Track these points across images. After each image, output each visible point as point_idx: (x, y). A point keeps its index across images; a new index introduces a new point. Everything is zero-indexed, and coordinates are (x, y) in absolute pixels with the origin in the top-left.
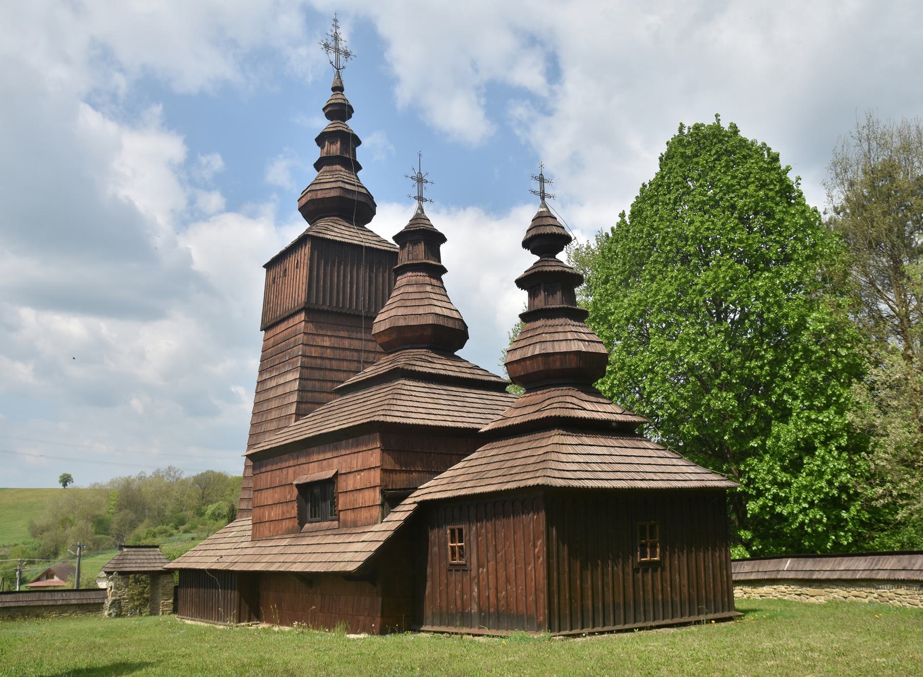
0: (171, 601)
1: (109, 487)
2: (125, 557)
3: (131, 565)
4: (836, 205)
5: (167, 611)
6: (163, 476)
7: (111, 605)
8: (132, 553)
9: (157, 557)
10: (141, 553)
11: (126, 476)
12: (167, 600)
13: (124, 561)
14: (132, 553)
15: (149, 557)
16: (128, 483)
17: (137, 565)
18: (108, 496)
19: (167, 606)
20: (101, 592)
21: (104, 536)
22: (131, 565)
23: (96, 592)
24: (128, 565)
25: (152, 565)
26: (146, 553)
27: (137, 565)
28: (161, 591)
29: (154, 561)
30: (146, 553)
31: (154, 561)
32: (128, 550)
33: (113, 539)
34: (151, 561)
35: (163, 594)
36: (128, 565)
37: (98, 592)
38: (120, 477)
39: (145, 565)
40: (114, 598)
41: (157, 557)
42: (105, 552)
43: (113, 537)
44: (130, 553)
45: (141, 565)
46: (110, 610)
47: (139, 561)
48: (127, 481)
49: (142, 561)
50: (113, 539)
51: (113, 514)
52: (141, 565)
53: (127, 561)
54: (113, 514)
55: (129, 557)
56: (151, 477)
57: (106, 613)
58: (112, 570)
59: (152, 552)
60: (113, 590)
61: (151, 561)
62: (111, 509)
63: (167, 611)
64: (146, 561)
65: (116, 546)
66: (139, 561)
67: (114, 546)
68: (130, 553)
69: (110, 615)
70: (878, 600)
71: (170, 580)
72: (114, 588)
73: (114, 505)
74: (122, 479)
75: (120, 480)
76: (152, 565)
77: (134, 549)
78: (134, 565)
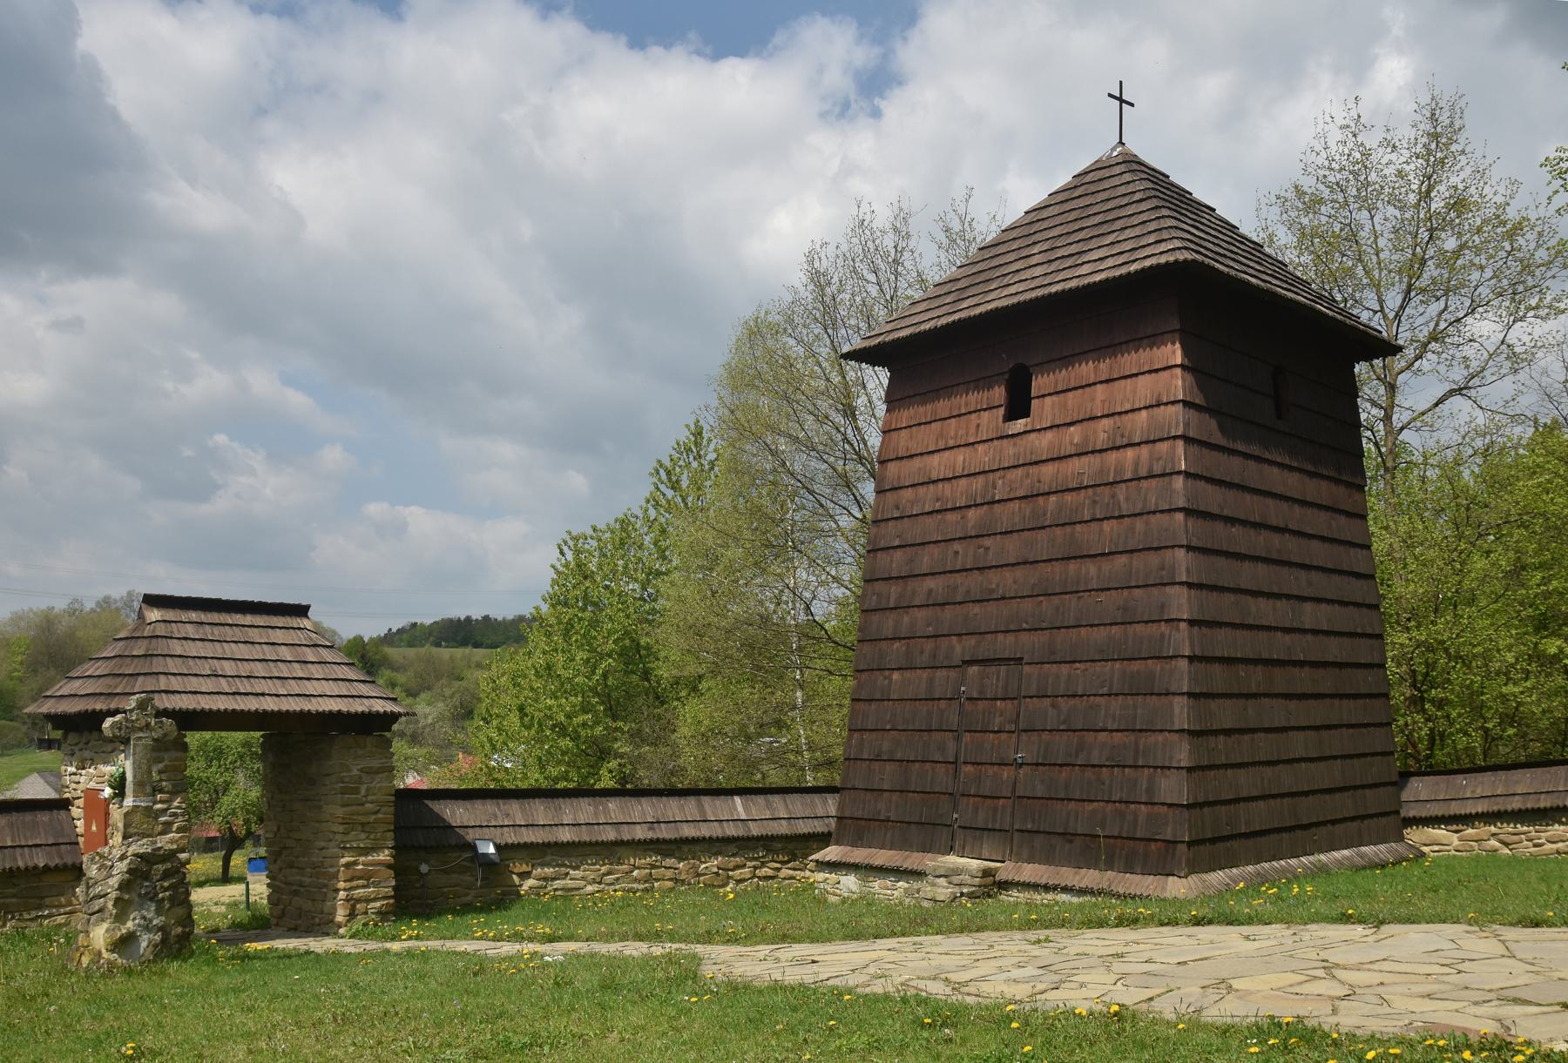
0: (385, 856)
1: (9, 629)
2: (161, 647)
3: (194, 684)
4: (1365, 109)
5: (368, 901)
6: (117, 609)
7: (123, 886)
8: (190, 631)
9: (310, 655)
10: (229, 633)
11: (44, 607)
12: (365, 851)
13: (158, 664)
14: (190, 631)
15: (269, 652)
16: (48, 621)
17: (224, 685)
18: (8, 645)
19: (366, 876)
20: (43, 817)
21: (8, 723)
22: (194, 684)
23: (15, 817)
24: (175, 684)
25: (295, 687)
26: (254, 635)
27: (224, 685)
28: (336, 809)
29: (298, 671)
30: (254, 635)
31: (298, 671)
32: (170, 615)
33: (24, 729)
34: (284, 670)
35: (349, 824)
36: (175, 684)
37: (28, 817)
38: (31, 610)
39: (261, 686)
40: (141, 847)
41: (310, 655)
42: (10, 752)
43: (25, 723)
44: (177, 630)
45: (244, 686)
46: (120, 918)
47: (228, 668)
48: (48, 621)
49: (244, 669)
50: (24, 729)
51: (21, 681)
52: (244, 686)
53: (172, 665)
54: (20, 680)
55: (177, 647)
56: (93, 610)
57: (100, 935)
58: (99, 706)
59: (281, 631)
60: (129, 802)
61: (284, 670)
62: (16, 670)
63: (368, 901)
64: (259, 669)
65: (32, 740)
66: (228, 668)
67: (26, 741)
68: (177, 630)
69: (124, 944)
70: (380, 816)
71: (375, 764)
72: (139, 785)
73: (21, 663)
74: (35, 614)
75: (31, 615)
76: (295, 687)
77: (193, 615)
78: (207, 685)
